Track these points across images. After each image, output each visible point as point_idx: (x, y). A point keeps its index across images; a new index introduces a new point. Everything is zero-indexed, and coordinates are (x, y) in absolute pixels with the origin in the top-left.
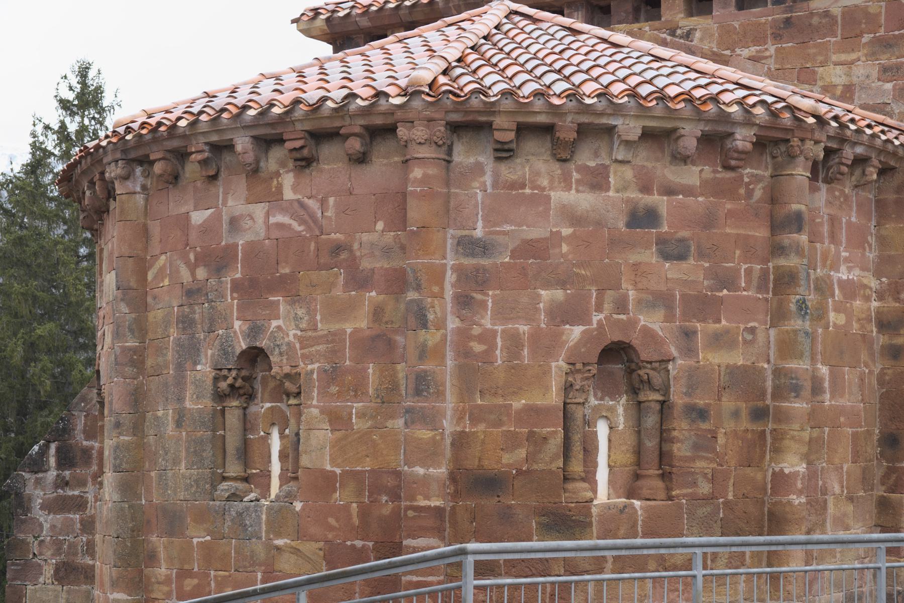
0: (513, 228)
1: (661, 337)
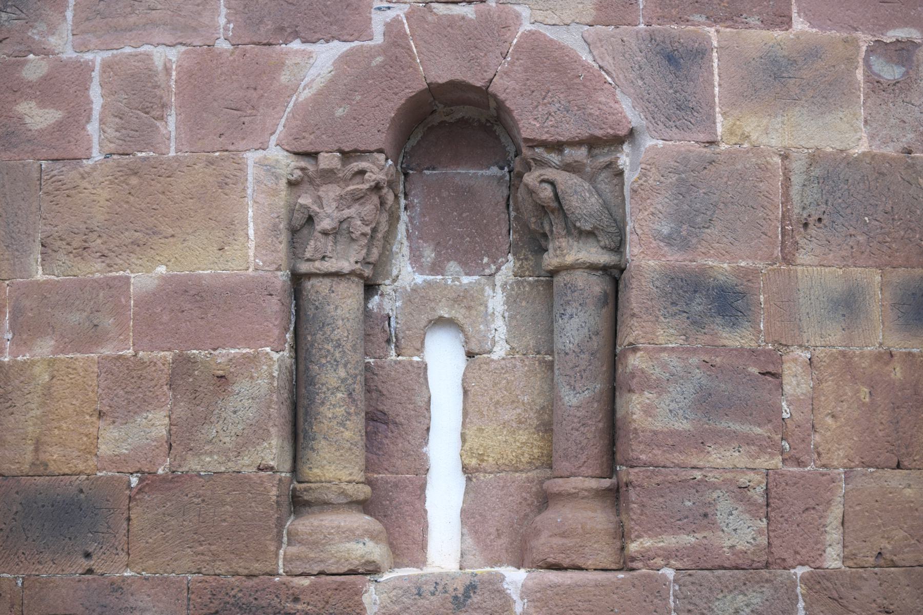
1: (586, 67)
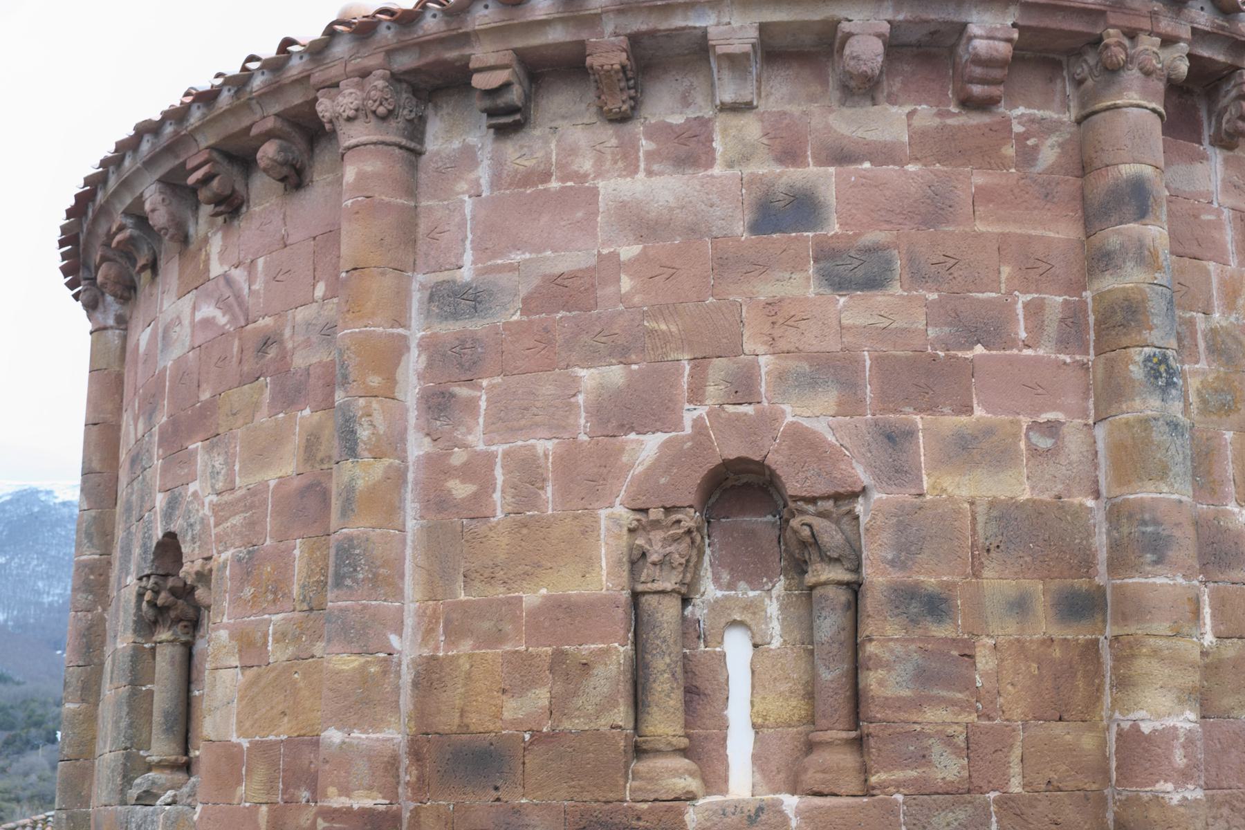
0: (527, 256)
1: (831, 446)
